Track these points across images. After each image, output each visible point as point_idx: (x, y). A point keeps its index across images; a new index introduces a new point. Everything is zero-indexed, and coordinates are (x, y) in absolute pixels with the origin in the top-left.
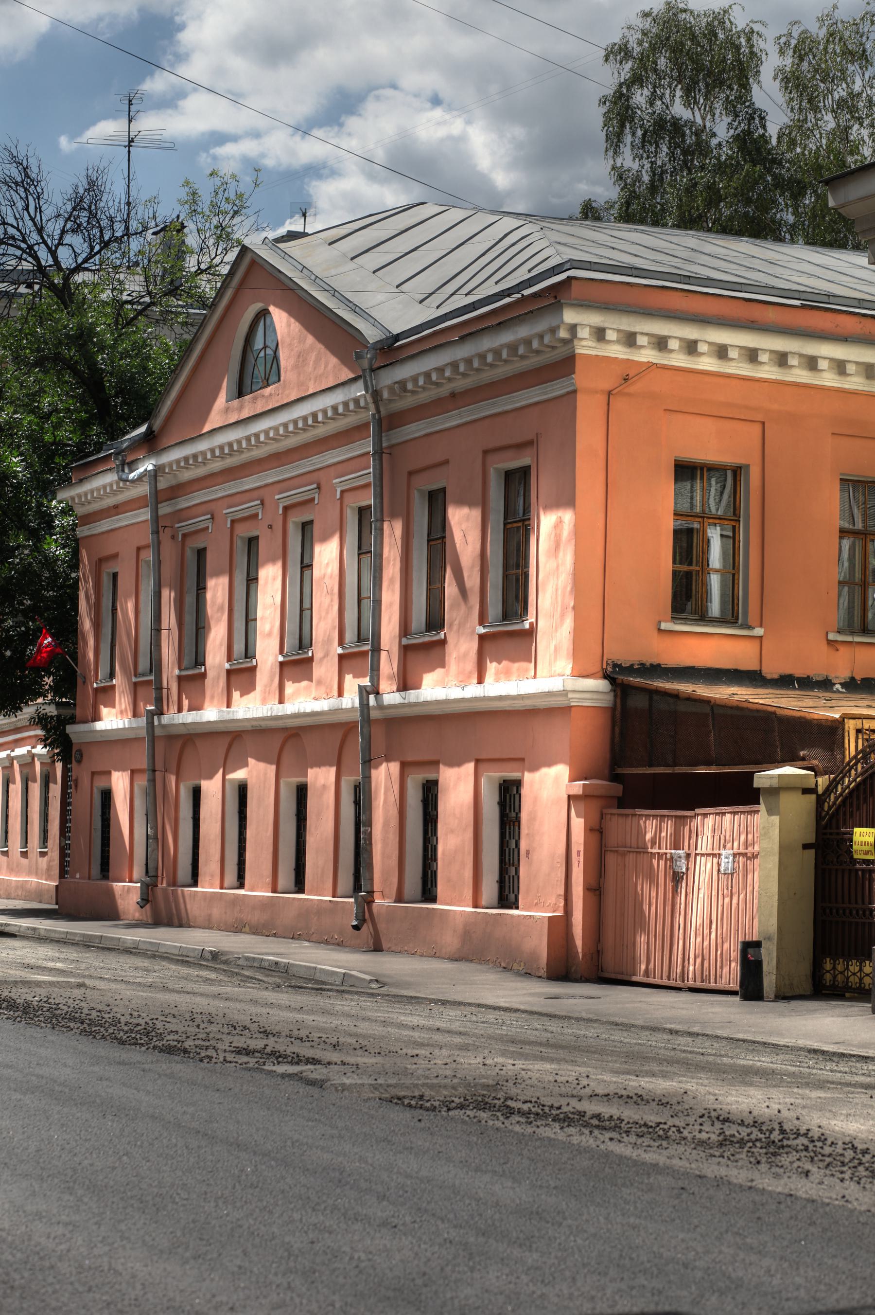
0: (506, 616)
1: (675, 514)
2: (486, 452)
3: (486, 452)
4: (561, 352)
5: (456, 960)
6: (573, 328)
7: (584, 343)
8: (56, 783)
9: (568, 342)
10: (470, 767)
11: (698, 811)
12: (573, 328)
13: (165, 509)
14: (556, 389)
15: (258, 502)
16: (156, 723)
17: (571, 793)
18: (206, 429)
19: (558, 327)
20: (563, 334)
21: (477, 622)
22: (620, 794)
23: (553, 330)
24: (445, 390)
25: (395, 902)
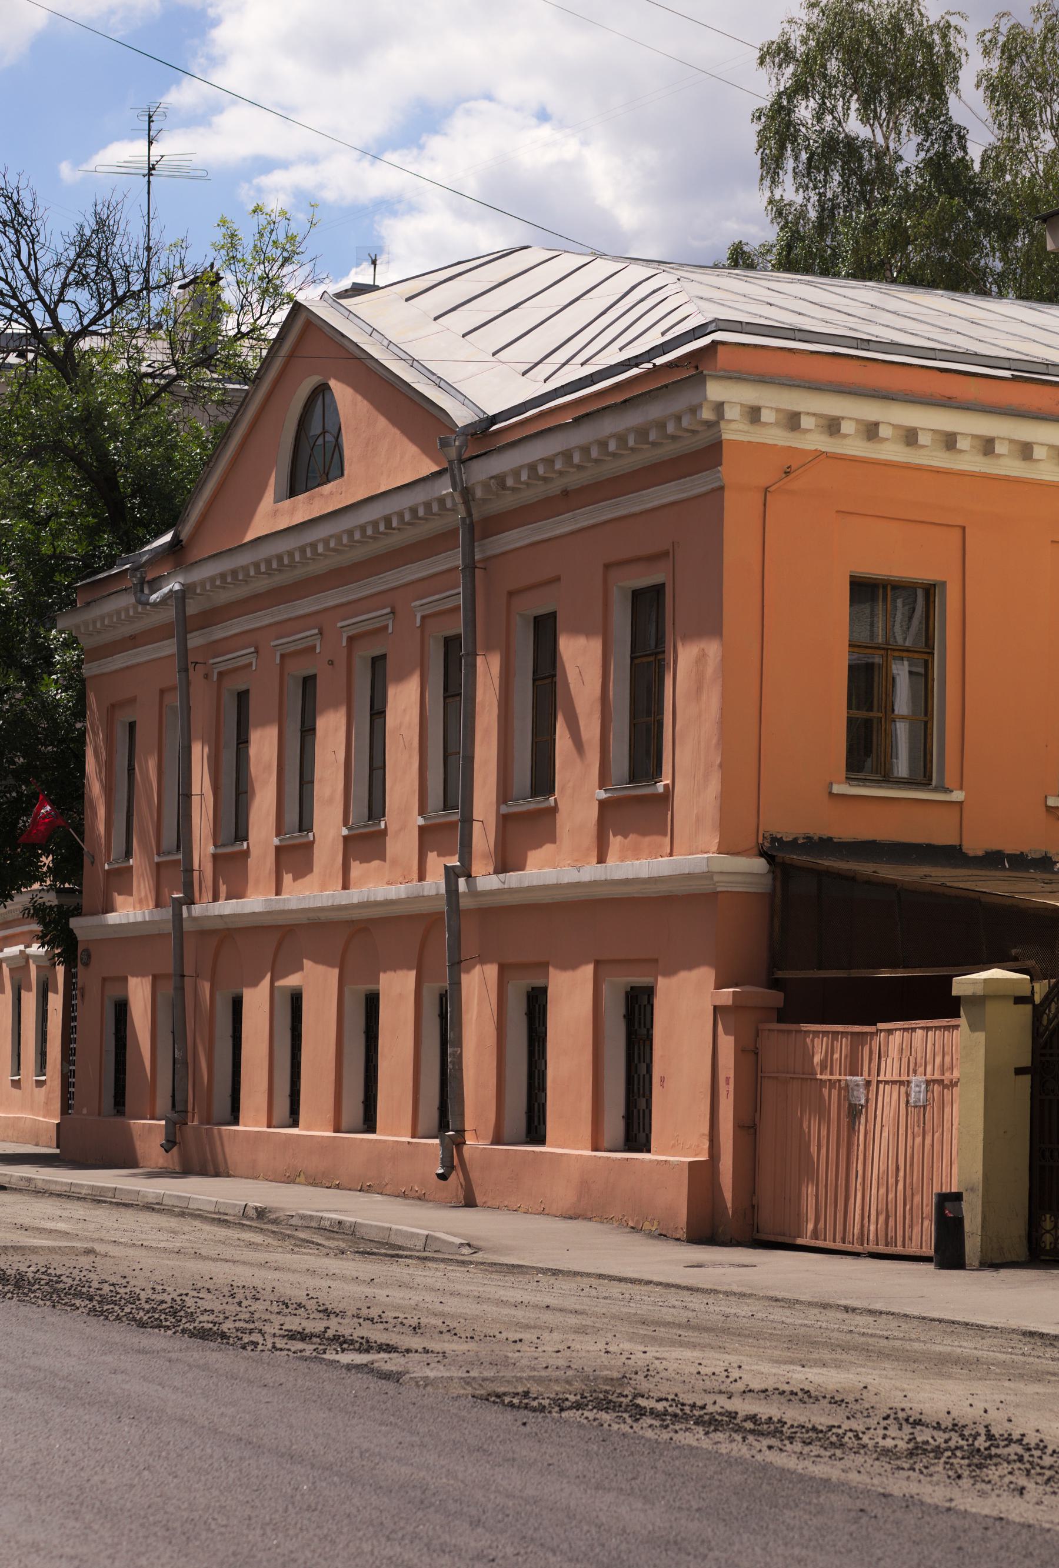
0: (634, 777)
1: (850, 646)
2: (607, 567)
3: (607, 567)
4: (704, 439)
5: (571, 1218)
6: (719, 407)
7: (734, 426)
8: (56, 992)
9: (713, 425)
10: (588, 970)
11: (881, 1026)
12: (719, 407)
13: (195, 640)
14: (696, 485)
15: (316, 631)
16: (185, 914)
17: (717, 1004)
18: (250, 536)
19: (700, 406)
20: (707, 414)
21: (597, 784)
22: (781, 1004)
23: (694, 410)
24: (555, 487)
25: (492, 1144)
